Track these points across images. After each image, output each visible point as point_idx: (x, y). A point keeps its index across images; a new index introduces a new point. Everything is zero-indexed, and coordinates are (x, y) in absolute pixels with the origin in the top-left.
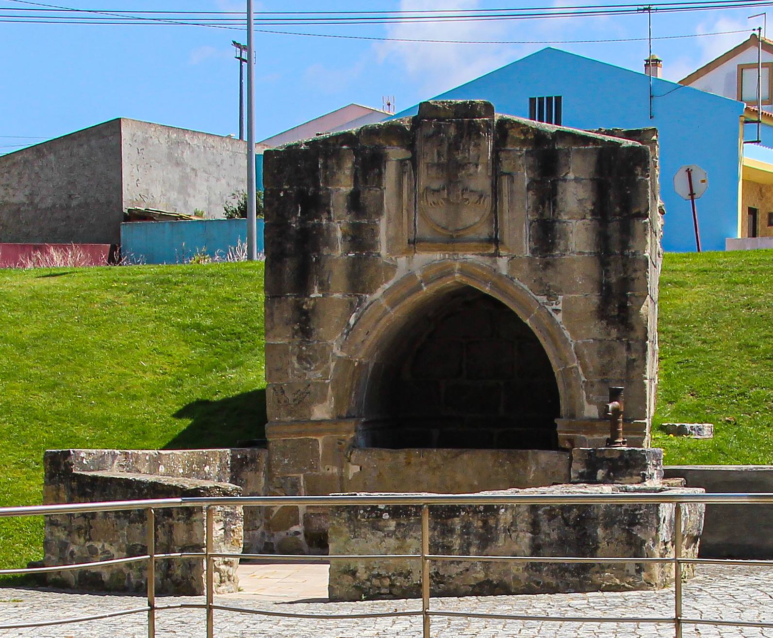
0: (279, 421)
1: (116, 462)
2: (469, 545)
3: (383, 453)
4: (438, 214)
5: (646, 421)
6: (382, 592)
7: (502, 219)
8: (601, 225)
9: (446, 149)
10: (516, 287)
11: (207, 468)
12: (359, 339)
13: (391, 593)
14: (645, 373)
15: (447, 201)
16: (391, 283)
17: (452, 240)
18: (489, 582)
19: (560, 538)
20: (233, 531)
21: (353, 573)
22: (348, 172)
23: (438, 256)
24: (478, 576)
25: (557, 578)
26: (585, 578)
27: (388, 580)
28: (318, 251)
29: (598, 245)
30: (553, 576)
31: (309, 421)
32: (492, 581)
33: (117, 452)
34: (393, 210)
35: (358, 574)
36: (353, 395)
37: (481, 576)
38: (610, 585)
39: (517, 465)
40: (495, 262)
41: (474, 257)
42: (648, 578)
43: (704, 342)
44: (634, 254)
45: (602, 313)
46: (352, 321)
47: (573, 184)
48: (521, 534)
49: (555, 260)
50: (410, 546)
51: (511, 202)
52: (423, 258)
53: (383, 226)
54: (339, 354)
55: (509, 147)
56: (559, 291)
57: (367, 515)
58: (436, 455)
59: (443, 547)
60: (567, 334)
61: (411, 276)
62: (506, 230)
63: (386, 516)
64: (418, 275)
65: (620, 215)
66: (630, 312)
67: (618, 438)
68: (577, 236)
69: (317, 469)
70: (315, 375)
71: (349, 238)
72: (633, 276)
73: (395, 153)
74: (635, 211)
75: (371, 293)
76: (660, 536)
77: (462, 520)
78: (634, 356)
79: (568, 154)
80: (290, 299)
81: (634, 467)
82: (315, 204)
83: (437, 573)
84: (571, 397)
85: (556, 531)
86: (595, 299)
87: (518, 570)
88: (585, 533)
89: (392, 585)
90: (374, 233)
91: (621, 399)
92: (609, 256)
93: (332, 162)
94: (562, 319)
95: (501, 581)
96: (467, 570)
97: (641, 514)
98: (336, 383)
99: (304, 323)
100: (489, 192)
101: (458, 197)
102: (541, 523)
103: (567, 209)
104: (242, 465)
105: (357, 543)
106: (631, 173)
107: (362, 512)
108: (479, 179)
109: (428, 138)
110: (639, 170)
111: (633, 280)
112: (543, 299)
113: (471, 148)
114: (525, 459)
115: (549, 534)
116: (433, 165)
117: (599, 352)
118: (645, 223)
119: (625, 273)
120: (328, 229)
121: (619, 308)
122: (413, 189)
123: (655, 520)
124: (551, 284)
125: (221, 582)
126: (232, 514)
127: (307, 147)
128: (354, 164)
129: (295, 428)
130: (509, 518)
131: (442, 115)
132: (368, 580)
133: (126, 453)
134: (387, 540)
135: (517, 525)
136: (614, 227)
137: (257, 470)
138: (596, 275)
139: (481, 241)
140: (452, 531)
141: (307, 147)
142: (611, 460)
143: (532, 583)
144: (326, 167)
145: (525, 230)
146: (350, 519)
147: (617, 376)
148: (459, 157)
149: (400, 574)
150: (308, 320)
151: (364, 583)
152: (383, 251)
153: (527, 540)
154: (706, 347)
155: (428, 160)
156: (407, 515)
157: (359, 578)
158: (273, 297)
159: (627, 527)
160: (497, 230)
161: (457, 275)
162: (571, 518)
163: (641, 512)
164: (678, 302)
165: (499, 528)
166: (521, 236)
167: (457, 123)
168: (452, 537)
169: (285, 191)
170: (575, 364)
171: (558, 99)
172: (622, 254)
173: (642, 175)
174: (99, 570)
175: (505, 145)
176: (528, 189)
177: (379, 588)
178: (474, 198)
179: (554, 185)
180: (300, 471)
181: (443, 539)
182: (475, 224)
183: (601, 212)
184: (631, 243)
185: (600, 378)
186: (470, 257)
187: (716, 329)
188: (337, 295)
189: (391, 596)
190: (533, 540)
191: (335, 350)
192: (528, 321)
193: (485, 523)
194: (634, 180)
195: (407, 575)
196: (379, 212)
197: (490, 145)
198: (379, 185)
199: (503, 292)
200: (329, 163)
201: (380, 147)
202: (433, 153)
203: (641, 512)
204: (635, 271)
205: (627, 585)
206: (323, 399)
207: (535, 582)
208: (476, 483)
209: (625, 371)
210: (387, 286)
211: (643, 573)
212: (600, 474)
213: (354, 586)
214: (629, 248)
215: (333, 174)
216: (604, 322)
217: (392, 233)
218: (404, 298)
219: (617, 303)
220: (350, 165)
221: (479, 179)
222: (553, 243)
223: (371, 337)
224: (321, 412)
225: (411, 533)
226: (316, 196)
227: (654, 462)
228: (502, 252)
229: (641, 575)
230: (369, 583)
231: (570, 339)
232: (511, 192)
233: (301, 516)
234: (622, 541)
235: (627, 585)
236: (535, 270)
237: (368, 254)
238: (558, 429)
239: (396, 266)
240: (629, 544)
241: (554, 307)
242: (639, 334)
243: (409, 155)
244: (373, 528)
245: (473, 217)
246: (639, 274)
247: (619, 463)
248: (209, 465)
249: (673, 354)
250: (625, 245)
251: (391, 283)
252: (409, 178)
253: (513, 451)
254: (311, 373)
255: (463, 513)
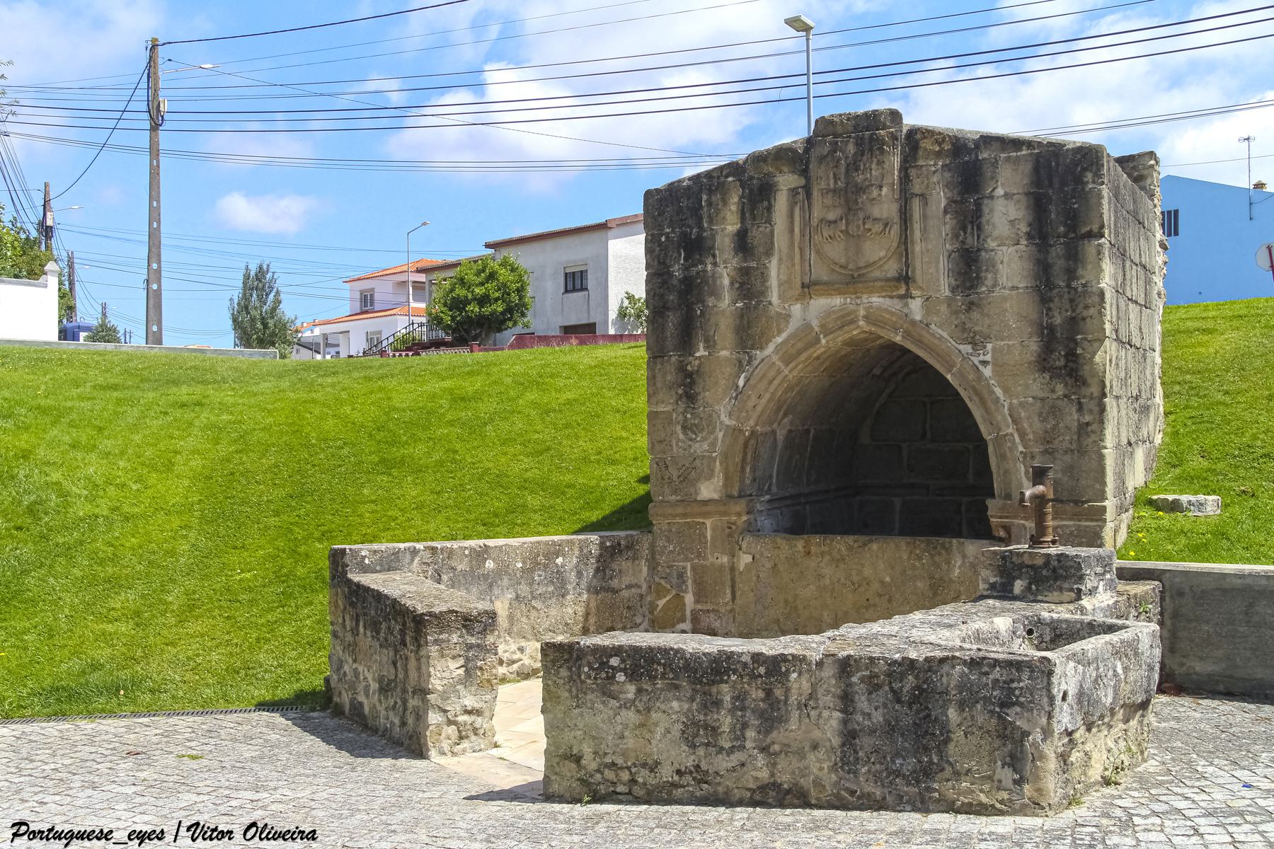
0: (662, 501)
1: (417, 560)
2: (745, 726)
3: (778, 540)
4: (836, 251)
5: (1106, 503)
6: (618, 790)
7: (913, 252)
8: (1039, 251)
9: (843, 170)
10: (933, 335)
11: (559, 561)
12: (750, 404)
13: (630, 793)
14: (1102, 440)
15: (846, 232)
16: (784, 335)
17: (853, 280)
18: (776, 786)
19: (888, 722)
20: (481, 668)
21: (578, 759)
22: (734, 208)
23: (837, 301)
24: (759, 775)
25: (883, 785)
26: (929, 789)
27: (627, 772)
28: (703, 302)
29: (1037, 277)
30: (876, 782)
31: (696, 500)
32: (781, 785)
33: (420, 546)
34: (785, 250)
35: (583, 762)
36: (748, 469)
37: (764, 775)
38: (970, 804)
39: (937, 558)
40: (906, 305)
41: (881, 300)
42: (1035, 794)
43: (1227, 393)
44: (1084, 286)
45: (1043, 363)
46: (741, 383)
47: (1001, 201)
48: (826, 714)
49: (981, 299)
50: (656, 725)
51: (924, 230)
52: (821, 304)
53: (773, 267)
54: (727, 421)
55: (921, 163)
56: (988, 337)
57: (593, 674)
58: (841, 544)
59: (706, 727)
60: (998, 391)
61: (807, 327)
62: (918, 265)
63: (621, 677)
64: (815, 324)
65: (1065, 236)
66: (1081, 361)
67: (1044, 535)
68: (1009, 265)
69: (705, 558)
70: (701, 447)
71: (737, 285)
72: (1085, 313)
73: (786, 181)
74: (1085, 230)
75: (762, 349)
76: (1055, 725)
77: (733, 687)
78: (1087, 418)
79: (995, 164)
80: (673, 359)
81: (1066, 578)
82: (697, 247)
83: (698, 766)
84: (1006, 472)
85: (881, 711)
86: (1034, 346)
87: (821, 769)
88: (929, 715)
89: (633, 781)
90: (764, 277)
91: (1047, 482)
92: (1051, 289)
93: (717, 198)
94: (995, 375)
95: (796, 785)
96: (743, 765)
97: (1022, 688)
98: (725, 457)
99: (689, 386)
100: (896, 219)
101: (858, 227)
102: (857, 697)
103: (995, 233)
104: (612, 555)
105: (581, 715)
106: (1079, 181)
107: (586, 669)
108: (884, 205)
109: (822, 159)
110: (1089, 176)
111: (1084, 319)
112: (967, 349)
113: (874, 166)
114: (948, 550)
115: (869, 714)
116: (828, 191)
117: (1040, 415)
118: (1099, 245)
119: (1074, 311)
120: (713, 276)
121: (1066, 356)
122: (806, 223)
123: (1046, 699)
124: (976, 328)
125: (461, 738)
126: (478, 646)
127: (690, 183)
128: (741, 197)
129: (680, 510)
130: (806, 686)
131: (839, 129)
132: (598, 771)
133: (433, 549)
134: (624, 712)
135: (817, 699)
136: (1057, 252)
137: (635, 559)
138: (1034, 316)
139: (888, 280)
140: (718, 704)
141: (690, 183)
142: (1032, 567)
143: (842, 792)
144: (710, 204)
145: (943, 263)
146: (571, 678)
147: (1066, 445)
148: (860, 179)
149: (644, 765)
150: (693, 383)
151: (591, 776)
152: (775, 298)
153: (834, 723)
154: (1228, 399)
155: (823, 185)
156: (650, 677)
157: (584, 768)
158: (655, 358)
159: (997, 709)
160: (907, 266)
161: (861, 323)
162: (905, 690)
163: (1022, 684)
164: (1203, 350)
165: (790, 702)
166: (937, 271)
167: (857, 138)
168: (718, 713)
169: (667, 236)
170: (1010, 430)
171: (1176, 212)
172: (1069, 286)
173: (1094, 182)
174: (830, 560)
175: (916, 160)
176: (946, 212)
177: (614, 784)
178: (878, 227)
179: (978, 204)
180: (686, 559)
181: (705, 715)
182: (880, 259)
183: (1039, 234)
184: (1080, 272)
185: (1042, 448)
186: (876, 300)
187: (1243, 378)
188: (724, 353)
189: (631, 798)
190: (845, 722)
191: (723, 416)
192: (949, 377)
193: (769, 693)
194: (1083, 189)
195: (654, 767)
196: (769, 253)
197: (896, 161)
198: (769, 221)
199: (919, 342)
200: (714, 199)
201: (769, 175)
202: (828, 178)
203: (1022, 684)
204: (1087, 307)
205: (998, 805)
206: (711, 476)
207: (847, 789)
208: (888, 579)
209: (1075, 437)
210: (779, 340)
211: (1026, 787)
212: (1019, 586)
213: (578, 779)
214: (1078, 279)
215: (718, 211)
216: (1047, 375)
217: (783, 277)
218: (800, 353)
219: (1065, 351)
220: (736, 200)
221: (884, 205)
222: (978, 277)
223: (764, 401)
224: (708, 490)
225: (658, 704)
226: (700, 238)
227: (1099, 570)
228: (915, 292)
229: (1022, 790)
230: (598, 776)
231: (1002, 398)
232: (925, 217)
233: (688, 613)
234: (988, 732)
235: (998, 805)
236: (956, 313)
237: (758, 303)
238: (989, 513)
239: (790, 316)
240: (1003, 737)
241: (982, 358)
242: (1094, 390)
243: (803, 182)
244: (604, 694)
245: (878, 251)
246: (1092, 311)
247: (1044, 572)
248: (564, 556)
249: (1186, 407)
250: (1071, 274)
251: (784, 335)
252: (802, 209)
253: (933, 539)
254: (697, 445)
255: (734, 678)
